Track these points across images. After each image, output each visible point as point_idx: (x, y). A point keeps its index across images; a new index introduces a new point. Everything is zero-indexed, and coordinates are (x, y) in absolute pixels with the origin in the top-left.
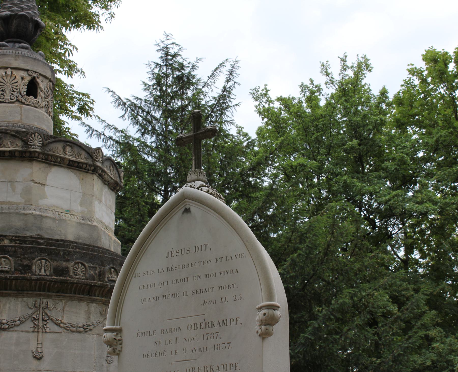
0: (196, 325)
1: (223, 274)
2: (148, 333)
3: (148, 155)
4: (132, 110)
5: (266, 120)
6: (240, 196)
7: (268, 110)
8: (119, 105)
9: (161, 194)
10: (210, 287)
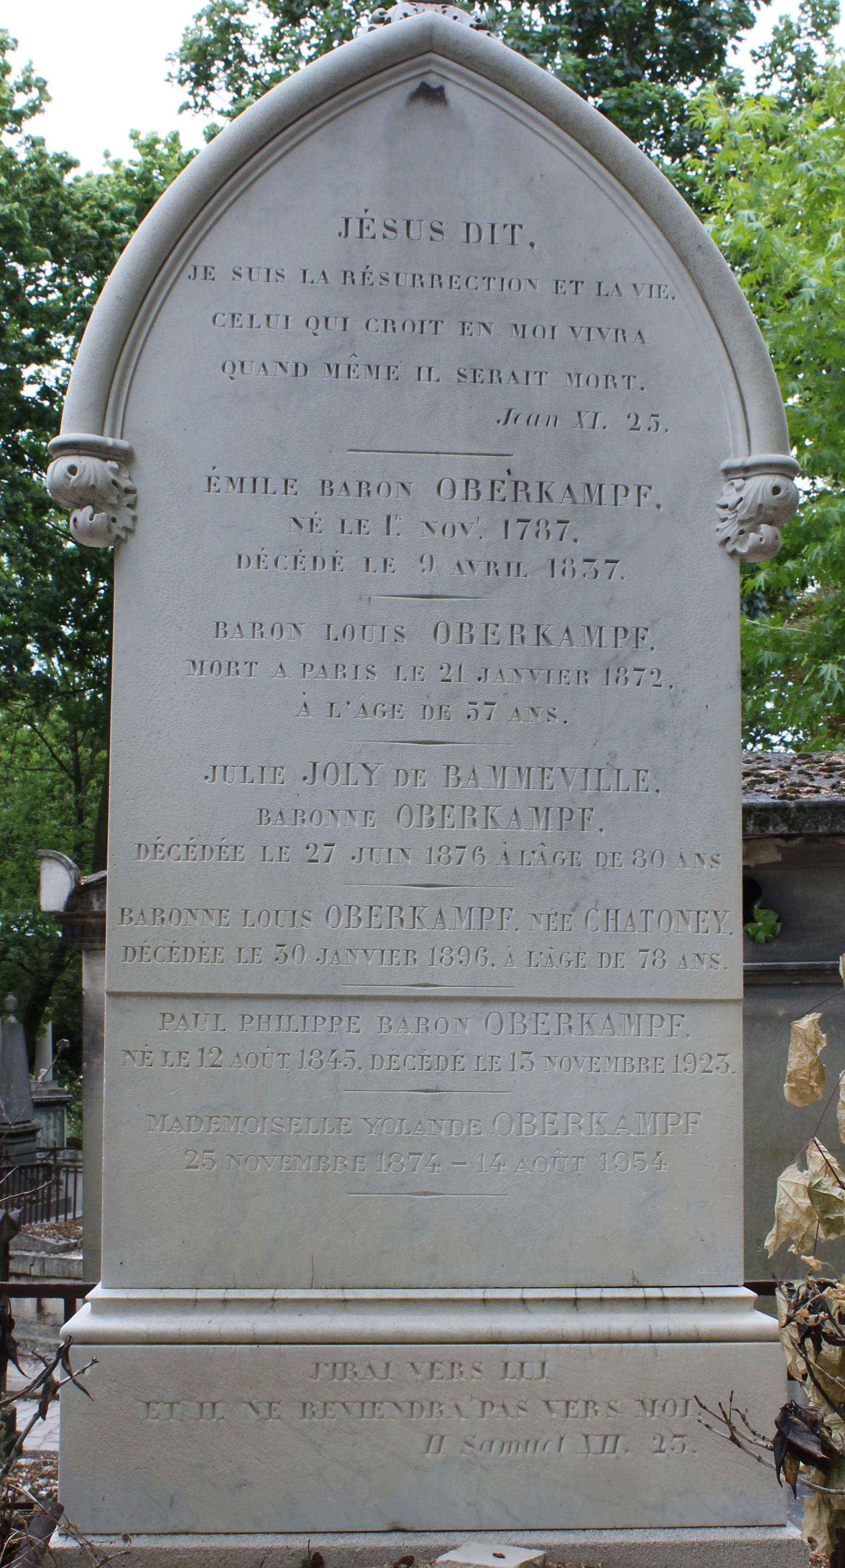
2: (258, 484)
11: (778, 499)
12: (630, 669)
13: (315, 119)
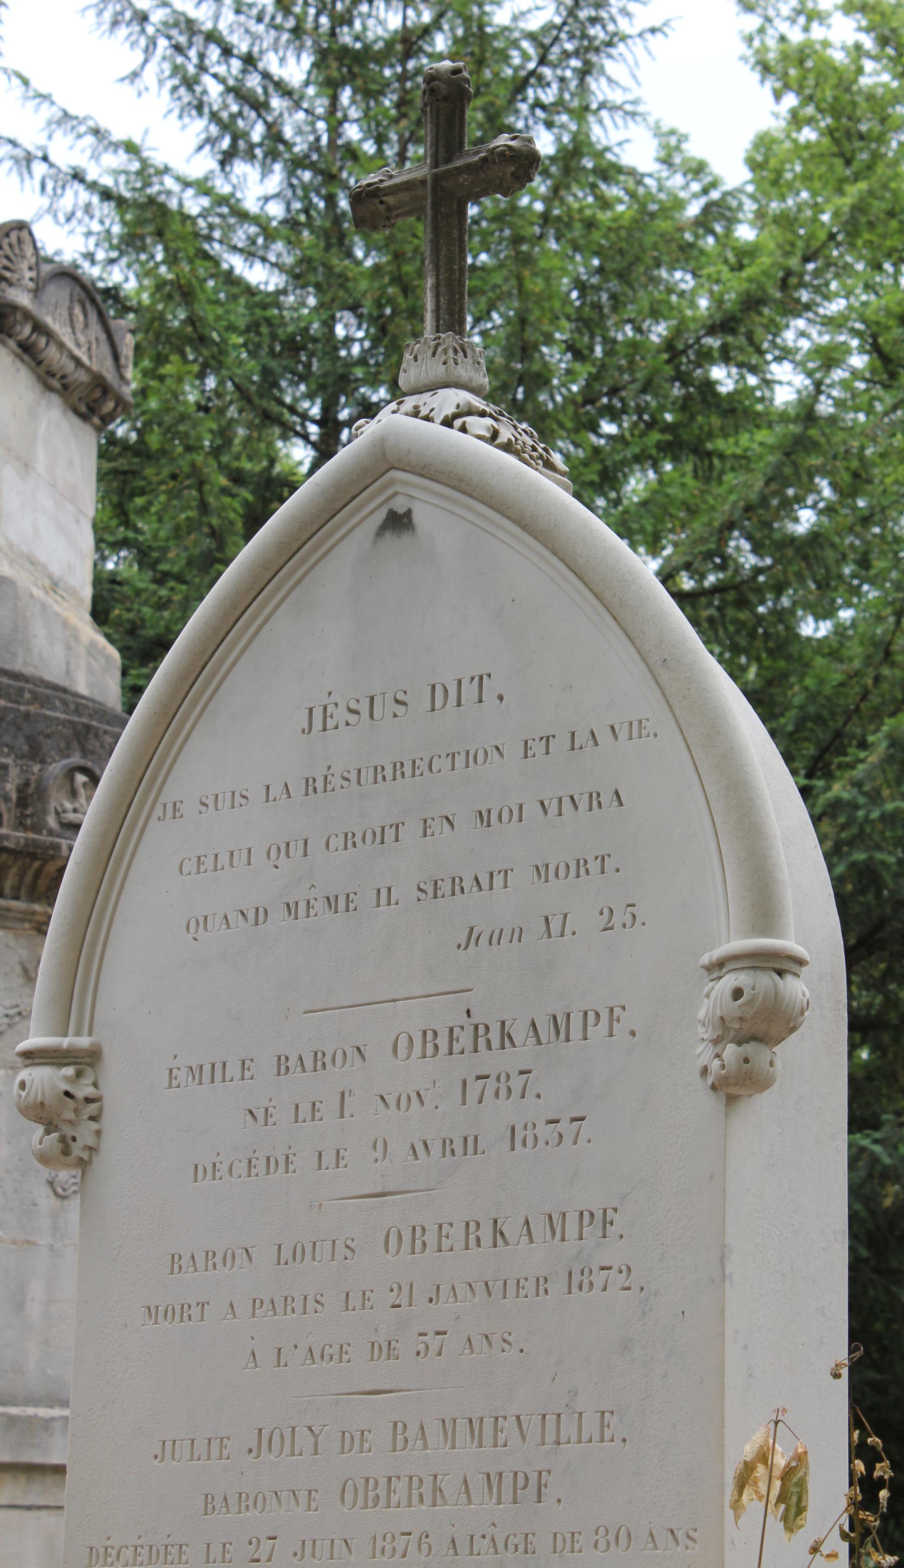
0: (430, 1035)
1: (553, 809)
2: (216, 1072)
3: (250, 253)
4: (178, 48)
5: (791, 100)
6: (662, 447)
7: (800, 56)
8: (115, 23)
9: (305, 437)
10: (496, 869)
11: (740, 1006)
12: (595, 1270)
13: (278, 589)
